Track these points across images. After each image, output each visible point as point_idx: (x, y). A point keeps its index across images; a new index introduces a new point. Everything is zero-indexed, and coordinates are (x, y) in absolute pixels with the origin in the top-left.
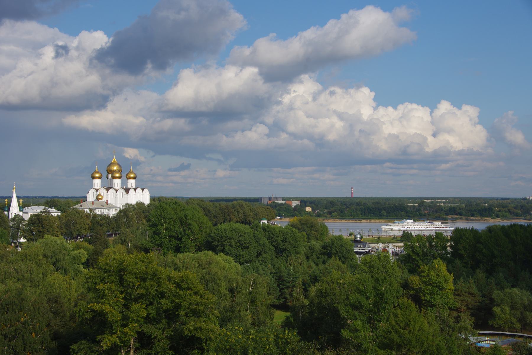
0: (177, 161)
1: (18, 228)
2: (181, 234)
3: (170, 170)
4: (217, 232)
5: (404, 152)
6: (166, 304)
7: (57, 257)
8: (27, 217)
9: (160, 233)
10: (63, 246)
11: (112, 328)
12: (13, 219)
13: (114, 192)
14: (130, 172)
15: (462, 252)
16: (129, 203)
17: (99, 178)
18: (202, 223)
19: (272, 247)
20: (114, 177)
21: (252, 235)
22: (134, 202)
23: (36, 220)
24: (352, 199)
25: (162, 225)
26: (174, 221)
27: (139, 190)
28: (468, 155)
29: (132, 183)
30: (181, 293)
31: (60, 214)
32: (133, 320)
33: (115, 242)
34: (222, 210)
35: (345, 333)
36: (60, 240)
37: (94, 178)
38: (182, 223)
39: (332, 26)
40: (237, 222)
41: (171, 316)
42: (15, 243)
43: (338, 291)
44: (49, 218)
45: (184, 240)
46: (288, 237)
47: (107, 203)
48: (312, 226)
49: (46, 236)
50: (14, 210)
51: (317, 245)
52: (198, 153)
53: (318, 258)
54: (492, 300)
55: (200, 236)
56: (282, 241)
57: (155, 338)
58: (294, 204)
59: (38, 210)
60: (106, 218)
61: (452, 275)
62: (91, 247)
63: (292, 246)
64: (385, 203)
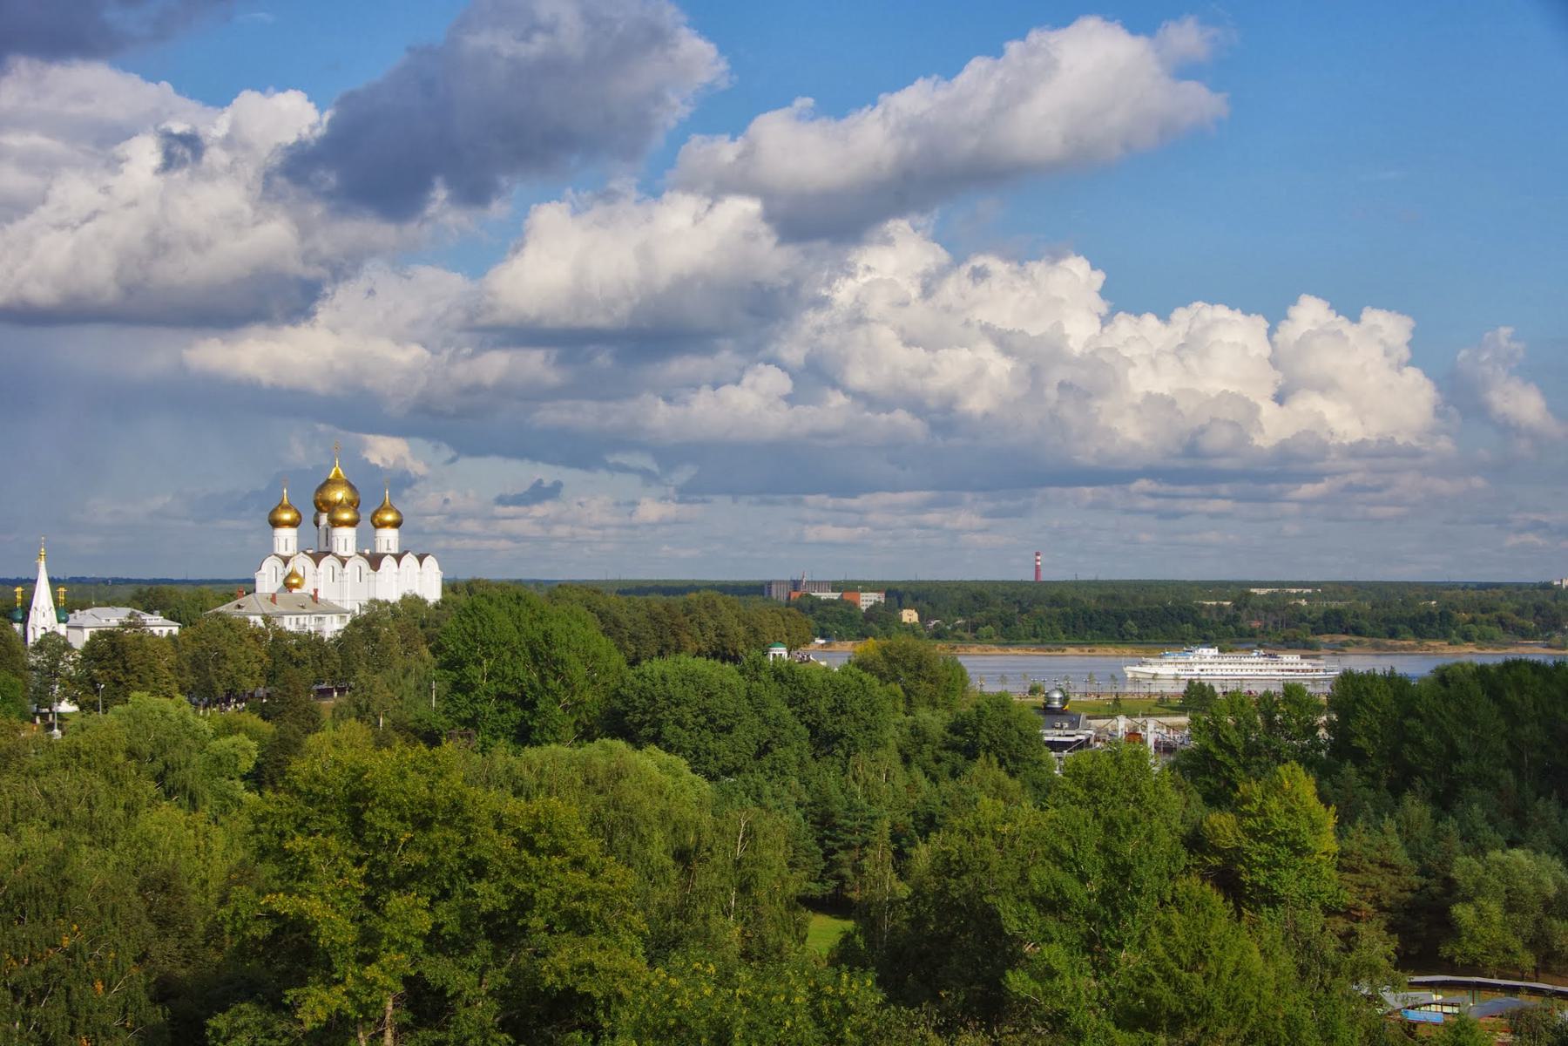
0: (520, 474)
1: (52, 671)
2: (532, 688)
3: (502, 501)
4: (640, 684)
5: (1192, 449)
6: (488, 895)
7: (167, 757)
8: (80, 640)
9: (473, 687)
10: (186, 724)
11: (329, 966)
12: (39, 647)
13: (337, 564)
14: (383, 508)
15: (1363, 742)
16: (381, 597)
17: (292, 524)
18: (596, 656)
19: (802, 729)
20: (335, 523)
21: (744, 693)
22: (394, 596)
23: (107, 649)
24: (1038, 585)
25: (479, 663)
26: (514, 653)
27: (410, 560)
28: (1379, 456)
29: (388, 539)
30: (533, 862)
31: (176, 630)
32: (393, 942)
33: (339, 715)
34: (654, 618)
35: (1018, 982)
36: (177, 707)
37: (276, 524)
38: (535, 656)
39: (979, 79)
40: (699, 653)
41: (504, 930)
42: (44, 717)
43: (995, 858)
44: (144, 640)
45: (541, 706)
46: (848, 697)
47: (315, 598)
48: (920, 667)
49: (135, 696)
50: (43, 618)
51: (934, 721)
52: (585, 452)
53: (938, 760)
54: (1449, 884)
55: (588, 696)
56: (832, 710)
57: (458, 995)
58: (867, 600)
59: (111, 618)
60: (313, 643)
61: (1333, 809)
62: (268, 728)
63: (862, 724)
64: (1134, 599)
